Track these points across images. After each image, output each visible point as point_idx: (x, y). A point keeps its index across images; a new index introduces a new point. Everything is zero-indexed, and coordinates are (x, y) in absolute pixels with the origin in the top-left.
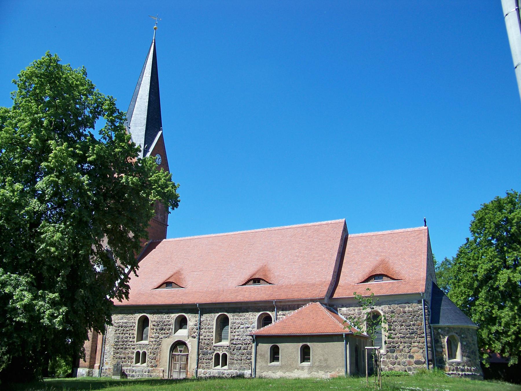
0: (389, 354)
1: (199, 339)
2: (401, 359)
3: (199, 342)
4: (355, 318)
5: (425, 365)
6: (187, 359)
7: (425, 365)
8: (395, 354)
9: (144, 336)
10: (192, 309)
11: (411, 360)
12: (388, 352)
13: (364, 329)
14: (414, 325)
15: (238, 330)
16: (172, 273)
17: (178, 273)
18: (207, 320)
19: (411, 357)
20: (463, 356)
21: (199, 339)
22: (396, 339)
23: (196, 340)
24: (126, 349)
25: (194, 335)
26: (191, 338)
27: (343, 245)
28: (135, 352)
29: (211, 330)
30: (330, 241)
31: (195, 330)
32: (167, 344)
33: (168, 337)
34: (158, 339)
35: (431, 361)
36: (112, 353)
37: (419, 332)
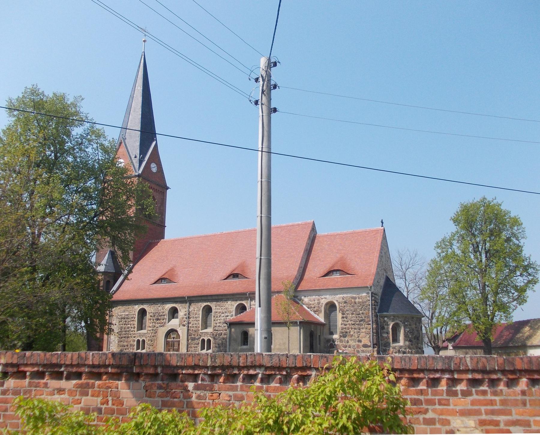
0: (342, 338)
1: (188, 327)
2: (351, 343)
3: (188, 330)
4: (314, 308)
5: (371, 349)
6: (179, 344)
7: (371, 349)
8: (346, 339)
9: (144, 326)
10: (181, 300)
11: (359, 344)
12: (341, 336)
13: (321, 318)
14: (363, 313)
15: (219, 318)
16: (167, 270)
17: (172, 270)
18: (194, 310)
19: (360, 341)
20: (405, 340)
21: (188, 327)
22: (348, 326)
23: (186, 328)
24: (128, 337)
25: (184, 323)
26: (181, 327)
27: (310, 243)
28: (136, 340)
29: (198, 319)
30: (299, 240)
31: (185, 319)
32: (162, 332)
33: (163, 326)
34: (155, 328)
35: (376, 344)
36: (117, 342)
37: (366, 320)
